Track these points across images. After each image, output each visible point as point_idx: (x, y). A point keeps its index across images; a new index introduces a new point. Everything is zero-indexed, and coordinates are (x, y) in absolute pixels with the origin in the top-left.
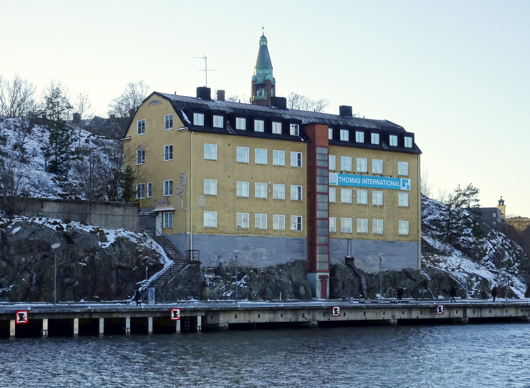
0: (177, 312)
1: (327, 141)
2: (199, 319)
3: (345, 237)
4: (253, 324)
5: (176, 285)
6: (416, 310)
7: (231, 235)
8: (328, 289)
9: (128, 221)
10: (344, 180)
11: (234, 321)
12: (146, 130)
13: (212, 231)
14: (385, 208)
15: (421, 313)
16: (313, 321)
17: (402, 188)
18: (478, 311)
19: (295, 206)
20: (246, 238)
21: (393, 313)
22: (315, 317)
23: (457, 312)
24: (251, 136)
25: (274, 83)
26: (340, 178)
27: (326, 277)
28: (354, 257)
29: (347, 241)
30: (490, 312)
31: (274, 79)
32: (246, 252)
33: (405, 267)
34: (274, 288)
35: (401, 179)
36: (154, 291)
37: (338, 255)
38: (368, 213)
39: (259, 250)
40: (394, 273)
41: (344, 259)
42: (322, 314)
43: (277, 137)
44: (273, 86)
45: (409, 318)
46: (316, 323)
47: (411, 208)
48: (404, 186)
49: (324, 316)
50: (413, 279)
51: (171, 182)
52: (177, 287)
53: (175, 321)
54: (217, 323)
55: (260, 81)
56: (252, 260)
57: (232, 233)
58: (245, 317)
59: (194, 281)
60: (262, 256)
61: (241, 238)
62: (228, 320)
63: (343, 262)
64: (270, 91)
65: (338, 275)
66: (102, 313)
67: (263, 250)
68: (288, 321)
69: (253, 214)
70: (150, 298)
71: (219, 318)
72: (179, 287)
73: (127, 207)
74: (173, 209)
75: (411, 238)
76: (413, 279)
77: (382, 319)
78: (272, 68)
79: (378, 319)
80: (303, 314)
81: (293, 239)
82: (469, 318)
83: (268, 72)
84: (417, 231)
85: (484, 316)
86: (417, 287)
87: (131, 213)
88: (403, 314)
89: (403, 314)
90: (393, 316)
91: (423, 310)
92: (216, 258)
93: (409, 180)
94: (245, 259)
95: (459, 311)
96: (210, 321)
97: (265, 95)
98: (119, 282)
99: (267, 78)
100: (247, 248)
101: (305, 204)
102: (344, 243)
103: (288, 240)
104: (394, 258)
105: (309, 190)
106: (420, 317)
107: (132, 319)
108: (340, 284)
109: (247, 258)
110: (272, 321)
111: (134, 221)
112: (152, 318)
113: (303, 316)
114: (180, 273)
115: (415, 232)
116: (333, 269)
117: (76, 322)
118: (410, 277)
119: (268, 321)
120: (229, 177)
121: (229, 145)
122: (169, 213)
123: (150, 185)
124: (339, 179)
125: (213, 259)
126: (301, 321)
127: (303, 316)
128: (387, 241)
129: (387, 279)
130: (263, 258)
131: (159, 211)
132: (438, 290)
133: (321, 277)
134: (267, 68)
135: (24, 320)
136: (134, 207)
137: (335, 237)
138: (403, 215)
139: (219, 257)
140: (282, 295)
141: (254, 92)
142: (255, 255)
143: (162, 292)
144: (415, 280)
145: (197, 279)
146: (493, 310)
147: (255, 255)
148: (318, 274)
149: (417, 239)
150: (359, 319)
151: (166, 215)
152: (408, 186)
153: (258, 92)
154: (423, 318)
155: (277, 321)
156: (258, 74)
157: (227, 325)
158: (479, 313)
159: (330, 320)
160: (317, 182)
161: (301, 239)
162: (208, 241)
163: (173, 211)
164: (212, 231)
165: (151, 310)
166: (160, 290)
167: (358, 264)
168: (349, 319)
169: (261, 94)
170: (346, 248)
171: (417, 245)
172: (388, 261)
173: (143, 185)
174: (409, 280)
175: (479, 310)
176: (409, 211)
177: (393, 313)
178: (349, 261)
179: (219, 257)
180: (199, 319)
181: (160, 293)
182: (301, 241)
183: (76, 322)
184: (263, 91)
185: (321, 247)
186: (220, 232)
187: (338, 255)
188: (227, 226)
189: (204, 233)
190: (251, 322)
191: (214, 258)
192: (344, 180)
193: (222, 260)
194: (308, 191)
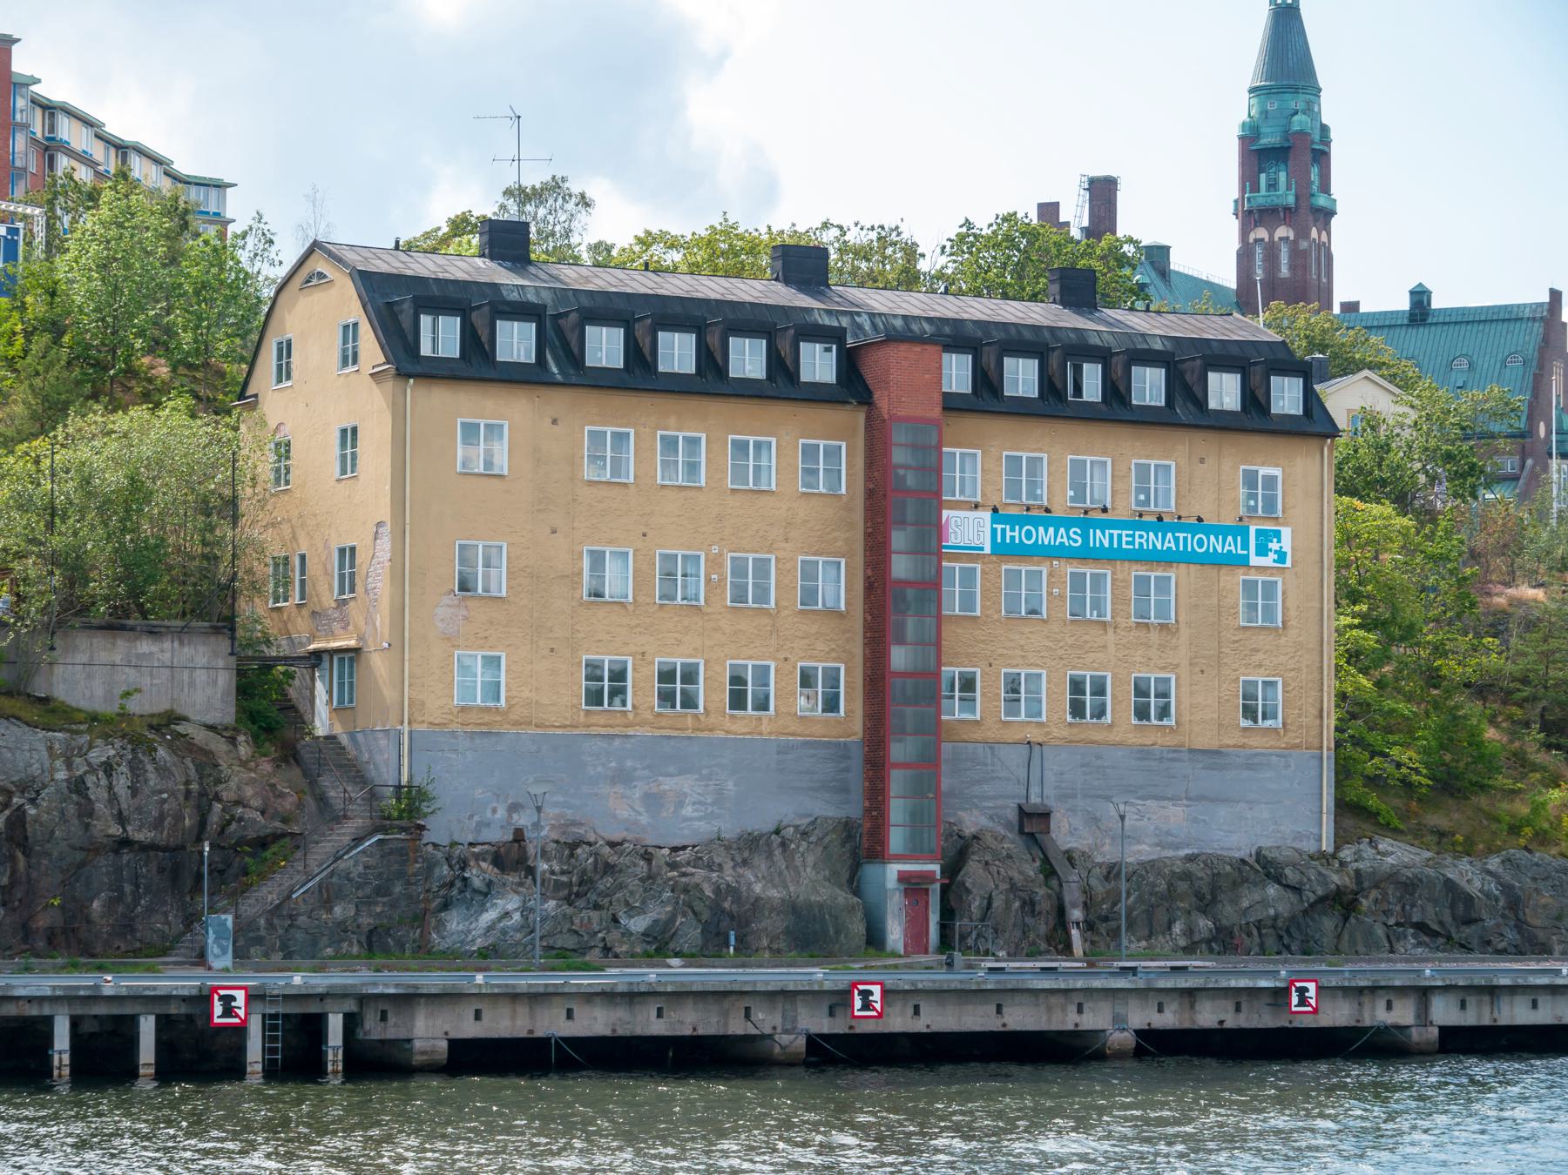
0: (870, 993)
1: (937, 398)
2: (335, 1024)
3: (1018, 737)
4: (545, 1042)
5: (327, 904)
6: (1213, 999)
7: (559, 731)
8: (934, 919)
9: (192, 684)
10: (1016, 534)
11: (470, 1030)
12: (294, 374)
13: (487, 718)
14: (1184, 632)
15: (1238, 1009)
16: (786, 1032)
17: (1255, 560)
18: (1479, 1003)
19: (814, 629)
20: (617, 742)
21: (1120, 1009)
22: (794, 1020)
23: (1389, 1006)
24: (655, 391)
25: (1328, 144)
26: (999, 527)
27: (927, 877)
28: (1051, 803)
29: (1024, 750)
30: (1535, 1005)
31: (1325, 129)
32: (619, 789)
33: (1265, 843)
34: (705, 916)
35: (1253, 529)
36: (230, 924)
37: (990, 798)
38: (1112, 649)
39: (668, 784)
40: (1209, 861)
41: (1012, 815)
42: (826, 1011)
43: (747, 391)
44: (1321, 157)
45: (1186, 1025)
46: (800, 1043)
47: (1293, 633)
48: (1262, 551)
49: (831, 1014)
50: (1287, 886)
51: (353, 549)
52: (330, 910)
53: (241, 1031)
54: (403, 1035)
55: (1269, 139)
56: (644, 819)
57: (565, 727)
58: (513, 1018)
59: (398, 889)
60: (680, 804)
61: (602, 744)
62: (447, 1027)
63: (1008, 825)
64: (1309, 173)
65: (973, 872)
66: (69, 998)
67: (687, 784)
68: (688, 1032)
69: (648, 658)
70: (213, 948)
71: (412, 1018)
72: (338, 910)
73: (186, 639)
74: (352, 643)
75: (1292, 738)
76: (1287, 886)
77: (1071, 1027)
78: (1318, 91)
79: (1054, 1027)
80: (747, 1010)
81: (806, 744)
82: (1444, 1030)
83: (1301, 106)
84: (1315, 712)
85: (1504, 1020)
86: (1305, 912)
87: (202, 660)
88: (1160, 1010)
89: (1160, 1010)
90: (1118, 1020)
91: (1243, 999)
92: (501, 813)
93: (1286, 532)
94: (614, 816)
95: (1397, 1004)
96: (373, 1029)
97: (1289, 188)
98: (120, 890)
99: (1296, 128)
100: (622, 777)
101: (858, 623)
102: (1015, 757)
103: (785, 749)
104: (1223, 812)
105: (869, 572)
106: (1229, 1024)
107: (75, 1023)
108: (976, 905)
109: (624, 813)
110: (620, 1032)
111: (215, 682)
112: (152, 1018)
113: (747, 1015)
114: (341, 865)
115: (1310, 719)
116: (958, 855)
117: (147, 1028)
118: (1278, 879)
119: (608, 1033)
120: (554, 532)
121: (554, 422)
122: (347, 656)
123: (303, 557)
124: (994, 531)
125: (489, 814)
126: (740, 1032)
127: (747, 1015)
128: (1191, 751)
129: (1182, 886)
130: (688, 811)
131: (326, 651)
132: (1398, 924)
133: (903, 878)
134: (1295, 90)
135: (237, 1016)
136: (212, 639)
137: (978, 736)
138: (1260, 656)
139: (514, 808)
140: (739, 939)
141: (1249, 179)
142: (653, 801)
143: (271, 926)
144: (1297, 890)
145: (408, 883)
146: (1543, 1000)
147: (653, 801)
148: (893, 870)
149: (1316, 742)
150: (978, 1028)
151: (341, 660)
152: (1281, 556)
153: (1263, 177)
154: (1245, 1025)
155: (639, 1031)
156: (1265, 113)
157: (444, 1044)
158: (1486, 1010)
159: (858, 1031)
160: (894, 546)
161: (838, 745)
162: (470, 755)
163: (357, 650)
164: (487, 718)
165: (959, 986)
166: (262, 922)
167: (1066, 833)
168: (935, 1028)
169: (1273, 186)
170: (1022, 773)
171: (1315, 763)
172: (1195, 820)
173: (286, 558)
174: (1272, 890)
175: (1487, 998)
176: (1283, 641)
177: (1120, 1009)
178: (1032, 823)
179: (514, 808)
180: (335, 1024)
181: (263, 932)
182: (840, 751)
183: (147, 1028)
184: (1282, 176)
185: (909, 772)
186: (516, 723)
187: (990, 798)
188: (545, 701)
189: (453, 727)
190: (539, 1034)
191: (494, 811)
192: (1016, 534)
193: (523, 820)
194: (867, 578)
